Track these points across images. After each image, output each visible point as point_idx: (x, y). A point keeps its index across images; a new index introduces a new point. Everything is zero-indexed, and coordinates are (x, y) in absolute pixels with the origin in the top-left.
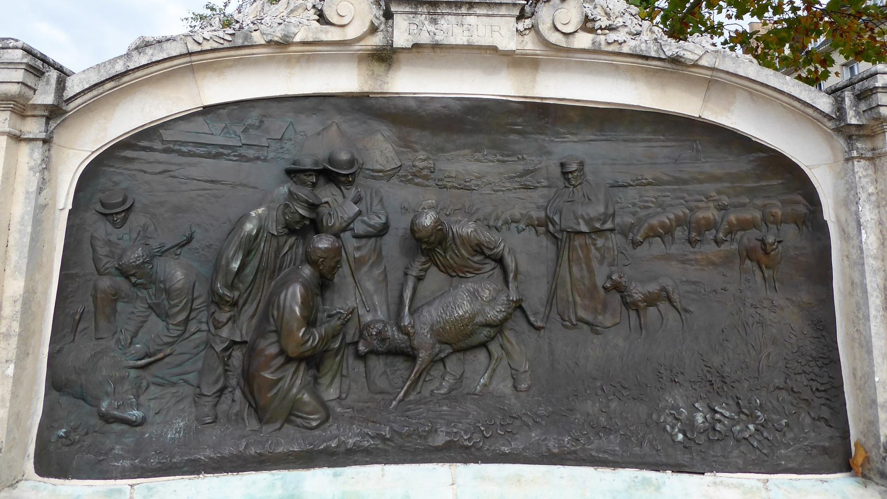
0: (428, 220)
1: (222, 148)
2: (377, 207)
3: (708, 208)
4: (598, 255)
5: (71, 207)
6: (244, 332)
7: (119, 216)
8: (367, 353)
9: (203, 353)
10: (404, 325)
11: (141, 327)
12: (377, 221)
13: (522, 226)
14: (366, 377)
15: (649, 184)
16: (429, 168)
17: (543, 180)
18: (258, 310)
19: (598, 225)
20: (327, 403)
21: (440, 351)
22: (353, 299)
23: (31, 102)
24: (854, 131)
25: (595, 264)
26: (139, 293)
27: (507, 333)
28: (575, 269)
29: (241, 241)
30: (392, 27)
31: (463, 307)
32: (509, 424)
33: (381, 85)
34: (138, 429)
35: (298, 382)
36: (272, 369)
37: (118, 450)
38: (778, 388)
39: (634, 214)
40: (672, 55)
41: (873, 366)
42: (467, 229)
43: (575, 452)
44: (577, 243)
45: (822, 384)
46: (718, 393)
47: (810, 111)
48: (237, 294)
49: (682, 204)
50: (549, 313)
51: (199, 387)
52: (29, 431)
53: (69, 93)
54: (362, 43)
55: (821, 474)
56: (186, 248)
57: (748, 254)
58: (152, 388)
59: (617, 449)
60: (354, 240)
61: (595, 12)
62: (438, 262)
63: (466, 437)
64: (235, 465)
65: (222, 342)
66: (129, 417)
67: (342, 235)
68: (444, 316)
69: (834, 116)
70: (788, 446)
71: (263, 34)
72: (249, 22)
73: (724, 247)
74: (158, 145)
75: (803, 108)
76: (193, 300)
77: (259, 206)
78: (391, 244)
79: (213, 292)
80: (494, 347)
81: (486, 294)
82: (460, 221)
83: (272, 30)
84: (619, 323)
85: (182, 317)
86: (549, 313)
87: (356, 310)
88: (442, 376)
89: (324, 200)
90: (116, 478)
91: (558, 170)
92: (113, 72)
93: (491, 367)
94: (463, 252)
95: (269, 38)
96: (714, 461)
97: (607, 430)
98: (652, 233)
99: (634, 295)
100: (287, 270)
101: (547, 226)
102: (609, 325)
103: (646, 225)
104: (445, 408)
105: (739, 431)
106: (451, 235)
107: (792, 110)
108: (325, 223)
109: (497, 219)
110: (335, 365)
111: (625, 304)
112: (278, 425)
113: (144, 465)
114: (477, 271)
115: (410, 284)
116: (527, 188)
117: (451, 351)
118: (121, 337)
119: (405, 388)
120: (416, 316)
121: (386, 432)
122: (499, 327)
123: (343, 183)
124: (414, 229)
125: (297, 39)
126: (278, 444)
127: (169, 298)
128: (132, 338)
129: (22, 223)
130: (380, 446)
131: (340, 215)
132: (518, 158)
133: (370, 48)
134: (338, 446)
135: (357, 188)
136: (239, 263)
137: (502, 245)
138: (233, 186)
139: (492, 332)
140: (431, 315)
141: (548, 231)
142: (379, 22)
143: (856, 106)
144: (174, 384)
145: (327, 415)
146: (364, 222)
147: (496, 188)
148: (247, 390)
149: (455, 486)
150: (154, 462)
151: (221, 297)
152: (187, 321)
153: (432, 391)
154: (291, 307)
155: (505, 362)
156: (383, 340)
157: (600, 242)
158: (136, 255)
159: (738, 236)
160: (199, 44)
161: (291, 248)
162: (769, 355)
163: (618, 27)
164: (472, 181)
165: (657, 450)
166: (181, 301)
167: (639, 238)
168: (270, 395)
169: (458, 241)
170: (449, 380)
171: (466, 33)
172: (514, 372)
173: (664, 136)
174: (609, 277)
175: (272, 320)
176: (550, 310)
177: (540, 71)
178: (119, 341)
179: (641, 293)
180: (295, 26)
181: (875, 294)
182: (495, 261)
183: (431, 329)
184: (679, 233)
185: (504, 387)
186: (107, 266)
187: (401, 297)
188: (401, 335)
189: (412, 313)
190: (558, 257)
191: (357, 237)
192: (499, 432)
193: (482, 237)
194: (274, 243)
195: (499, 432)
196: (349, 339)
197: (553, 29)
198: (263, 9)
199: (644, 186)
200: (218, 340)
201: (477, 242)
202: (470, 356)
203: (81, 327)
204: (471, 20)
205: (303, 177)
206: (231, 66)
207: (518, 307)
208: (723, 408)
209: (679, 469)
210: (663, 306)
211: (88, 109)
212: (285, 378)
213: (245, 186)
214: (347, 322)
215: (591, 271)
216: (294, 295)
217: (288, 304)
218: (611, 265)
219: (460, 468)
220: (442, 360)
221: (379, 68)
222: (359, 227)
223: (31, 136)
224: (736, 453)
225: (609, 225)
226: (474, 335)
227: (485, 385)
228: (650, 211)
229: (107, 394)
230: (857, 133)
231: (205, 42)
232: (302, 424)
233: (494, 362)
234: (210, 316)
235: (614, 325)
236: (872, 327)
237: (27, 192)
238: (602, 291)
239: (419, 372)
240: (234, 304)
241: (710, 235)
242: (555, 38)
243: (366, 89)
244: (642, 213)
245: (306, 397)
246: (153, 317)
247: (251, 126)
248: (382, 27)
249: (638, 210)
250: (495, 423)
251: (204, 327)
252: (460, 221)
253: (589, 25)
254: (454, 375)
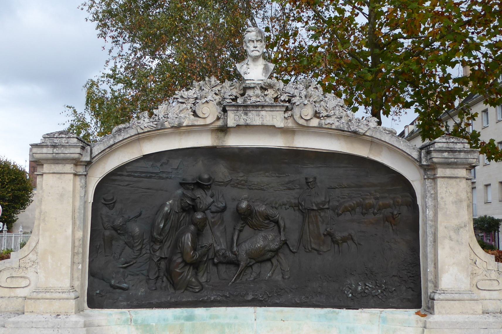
0: (244, 205)
1: (152, 174)
2: (221, 199)
5: (92, 201)
6: (166, 254)
7: (111, 205)
8: (218, 263)
9: (149, 262)
10: (234, 251)
11: (123, 251)
12: (221, 205)
13: (287, 207)
14: (218, 273)
15: (345, 187)
16: (244, 180)
17: (297, 186)
18: (171, 244)
19: (321, 207)
21: (250, 262)
22: (211, 240)
23: (81, 160)
24: (425, 167)
25: (320, 224)
26: (121, 237)
27: (280, 254)
28: (311, 226)
29: (163, 216)
30: (227, 116)
31: (260, 243)
32: (279, 292)
33: (222, 142)
34: (126, 291)
35: (190, 274)
37: (120, 298)
38: (394, 276)
39: (338, 201)
40: (354, 130)
41: (427, 265)
43: (306, 302)
44: (312, 214)
45: (412, 274)
46: (369, 278)
49: (359, 197)
50: (299, 246)
51: (148, 276)
53: (93, 155)
54: (213, 125)
55: (406, 309)
56: (138, 219)
57: (386, 219)
58: (129, 276)
59: (324, 300)
60: (211, 214)
61: (320, 109)
63: (260, 296)
64: (166, 305)
65: (157, 258)
66: (123, 286)
67: (206, 212)
68: (251, 247)
69: (418, 160)
71: (169, 123)
72: (162, 117)
73: (377, 216)
74: (125, 173)
75: (407, 156)
76: (144, 240)
78: (228, 215)
79: (152, 237)
80: (274, 261)
81: (270, 237)
82: (259, 205)
83: (173, 121)
84: (330, 250)
86: (299, 246)
87: (213, 245)
88: (251, 273)
89: (198, 196)
90: (122, 309)
92: (109, 145)
93: (273, 269)
94: (260, 219)
96: (363, 304)
97: (320, 293)
98: (346, 210)
99: (337, 237)
100: (182, 227)
101: (299, 207)
102: (326, 251)
103: (343, 206)
104: (252, 285)
105: (375, 293)
106: (254, 211)
108: (198, 207)
109: (276, 203)
112: (182, 291)
113: (132, 304)
114: (266, 227)
115: (237, 233)
117: (255, 262)
118: (115, 255)
119: (235, 277)
120: (239, 247)
122: (276, 252)
124: (238, 209)
125: (184, 124)
128: (120, 256)
129: (79, 209)
130: (225, 300)
131: (205, 203)
132: (286, 175)
133: (217, 126)
134: (207, 299)
135: (212, 191)
136: (163, 224)
137: (278, 215)
139: (273, 254)
140: (246, 247)
141: (299, 209)
142: (221, 114)
144: (138, 275)
145: (202, 288)
146: (215, 206)
147: (275, 189)
148: (169, 277)
149: (256, 313)
151: (156, 239)
152: (141, 249)
153: (247, 279)
154: (187, 242)
155: (279, 267)
158: (119, 222)
159: (383, 211)
160: (143, 129)
161: (184, 217)
162: (392, 263)
163: (331, 116)
164: (265, 186)
165: (340, 301)
166: (139, 241)
167: (340, 212)
168: (179, 278)
169: (258, 214)
170: (254, 275)
171: (261, 119)
172: (283, 271)
173: (352, 165)
174: (326, 230)
175: (179, 248)
176: (300, 244)
177: (296, 135)
178: (114, 257)
179: (340, 236)
180: (183, 119)
181: (430, 236)
182: (275, 222)
183: (246, 253)
184: (358, 210)
186: (108, 226)
187: (232, 239)
188: (233, 255)
189: (237, 246)
190: (304, 221)
191: (212, 212)
192: (275, 294)
193: (269, 212)
195: (275, 294)
196: (210, 257)
197: (300, 118)
198: (167, 109)
199: (343, 188)
200: (155, 257)
201: (266, 214)
203: (99, 251)
204: (263, 113)
205: (188, 186)
206: (155, 137)
207: (285, 243)
208: (370, 284)
209: (348, 308)
210: (350, 242)
211: (100, 160)
213: (162, 190)
214: (209, 250)
216: (188, 238)
217: (186, 241)
218: (327, 224)
220: (251, 266)
221: (221, 135)
222: (213, 208)
223: (81, 174)
225: (326, 206)
227: (270, 277)
229: (113, 278)
230: (427, 168)
231: (145, 128)
233: (274, 267)
235: (328, 250)
236: (428, 249)
237: (81, 197)
238: (323, 236)
239: (241, 270)
240: (161, 242)
241: (371, 211)
242: (301, 122)
243: (215, 145)
244: (342, 201)
245: (193, 280)
246: (127, 247)
247: (164, 163)
248: (222, 116)
249: (340, 199)
250: (273, 291)
251: (148, 251)
252: (259, 205)
253: (318, 115)
254: (256, 273)
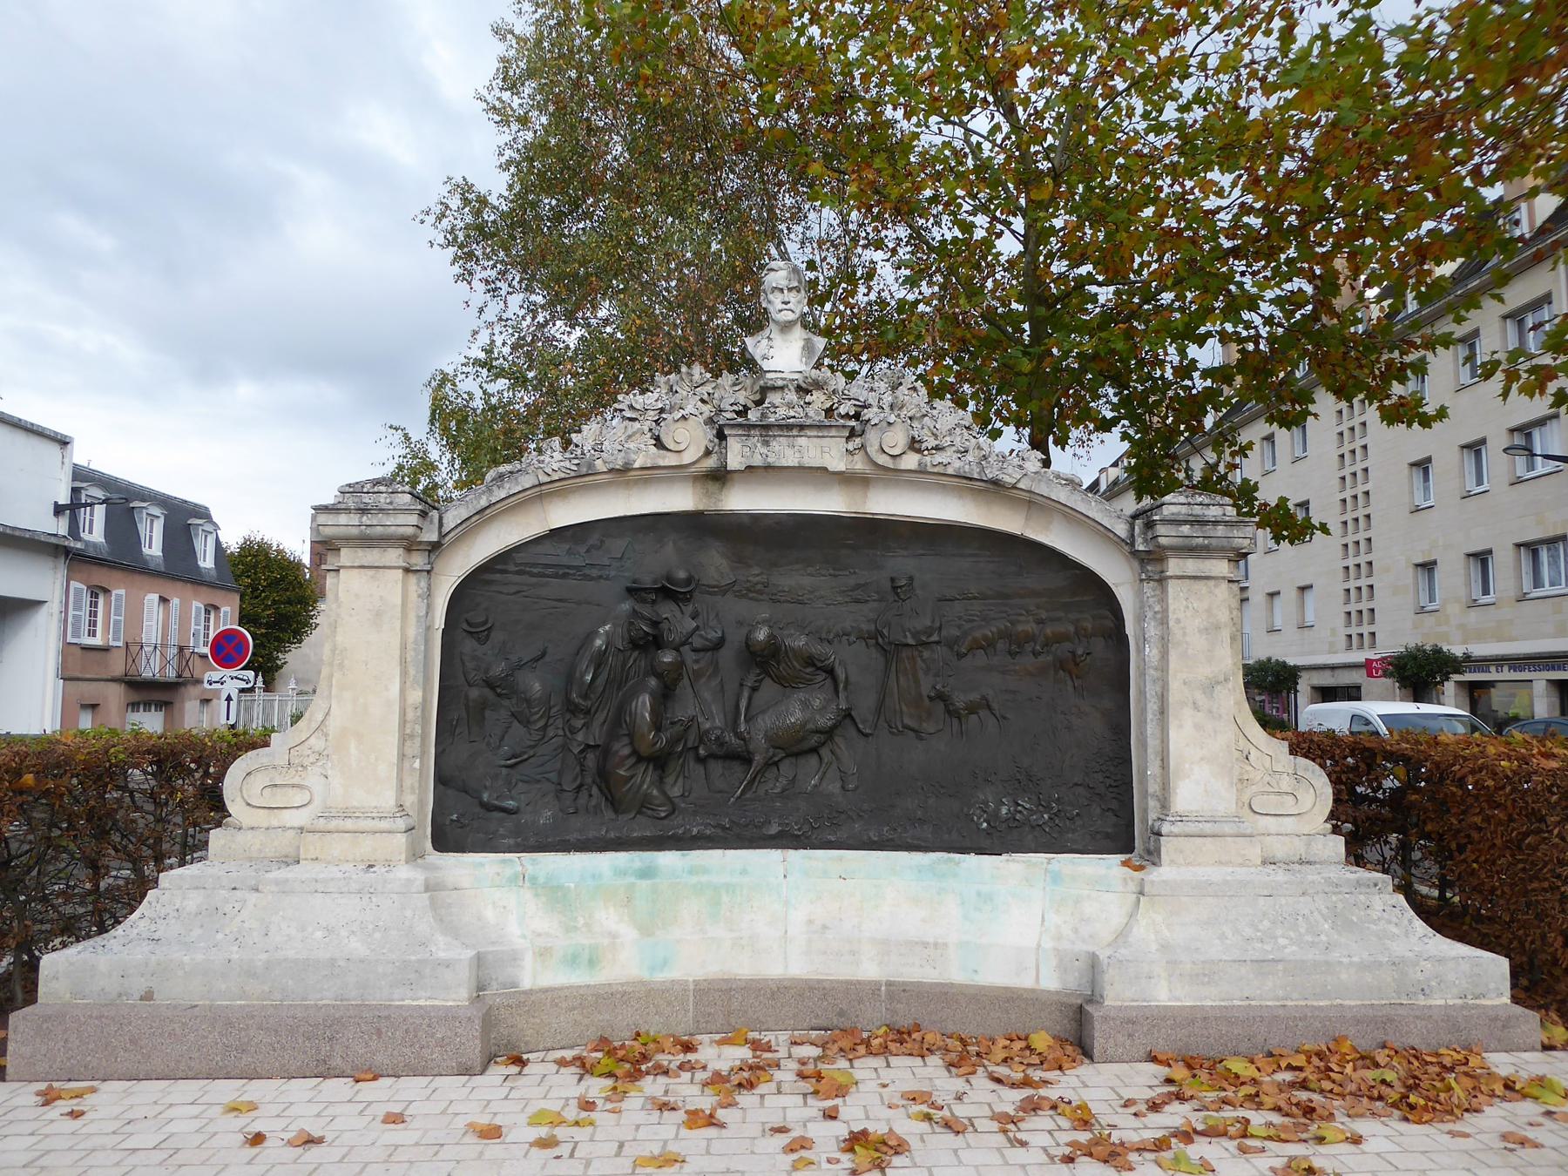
0: (761, 635)
2: (713, 623)
3: (1028, 622)
4: (923, 666)
12: (714, 635)
13: (853, 638)
15: (975, 598)
21: (774, 755)
25: (921, 674)
27: (837, 739)
28: (902, 679)
31: (795, 716)
35: (648, 779)
37: (501, 831)
38: (1076, 784)
39: (959, 627)
42: (799, 642)
43: (892, 840)
44: (904, 655)
47: (1111, 535)
48: (589, 703)
51: (560, 784)
52: (426, 816)
53: (446, 529)
57: (1061, 665)
58: (520, 784)
70: (1074, 831)
71: (605, 462)
73: (1041, 659)
74: (512, 568)
77: (604, 624)
78: (727, 656)
80: (825, 752)
81: (817, 703)
85: (541, 723)
91: (888, 585)
92: (479, 507)
95: (611, 466)
98: (976, 646)
107: (1098, 532)
109: (829, 632)
111: (949, 712)
114: (808, 682)
115: (746, 694)
116: (857, 601)
121: (726, 822)
122: (829, 733)
123: (682, 600)
124: (748, 644)
125: (636, 465)
127: (529, 707)
129: (416, 642)
138: (579, 603)
139: (823, 737)
141: (877, 643)
143: (1145, 534)
146: (701, 636)
148: (603, 785)
150: (532, 841)
151: (577, 706)
152: (546, 726)
155: (834, 766)
156: (722, 745)
157: (926, 654)
158: (498, 669)
170: (783, 781)
171: (797, 455)
184: (1000, 645)
185: (834, 787)
189: (747, 720)
191: (695, 650)
194: (621, 657)
196: (690, 744)
202: (802, 761)
204: (802, 441)
205: (644, 595)
207: (848, 715)
210: (983, 713)
211: (458, 540)
213: (589, 603)
215: (917, 682)
216: (644, 703)
218: (937, 675)
219: (792, 854)
220: (776, 764)
221: (713, 487)
222: (697, 642)
224: (1030, 837)
225: (935, 638)
226: (456, 269)
227: (815, 786)
228: (975, 624)
238: (927, 700)
240: (587, 712)
241: (1028, 647)
242: (882, 460)
243: (701, 507)
244: (967, 626)
245: (655, 792)
246: (516, 723)
248: (717, 448)
253: (917, 446)
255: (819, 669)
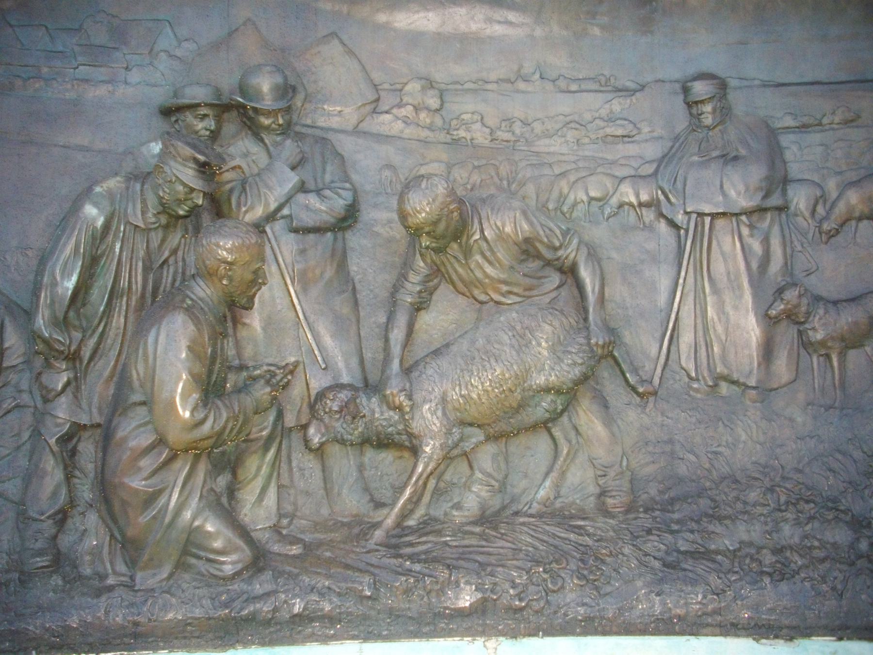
8: (322, 445)
20: (252, 534)
21: (461, 439)
36: (145, 474)
62: (454, 277)
87: (301, 367)
110: (264, 467)
115: (401, 320)
126: (165, 608)
136: (75, 278)
182: (561, 270)
202: (516, 446)
212: (168, 491)
232: (208, 572)
234: (34, 380)
255: (548, 263)
